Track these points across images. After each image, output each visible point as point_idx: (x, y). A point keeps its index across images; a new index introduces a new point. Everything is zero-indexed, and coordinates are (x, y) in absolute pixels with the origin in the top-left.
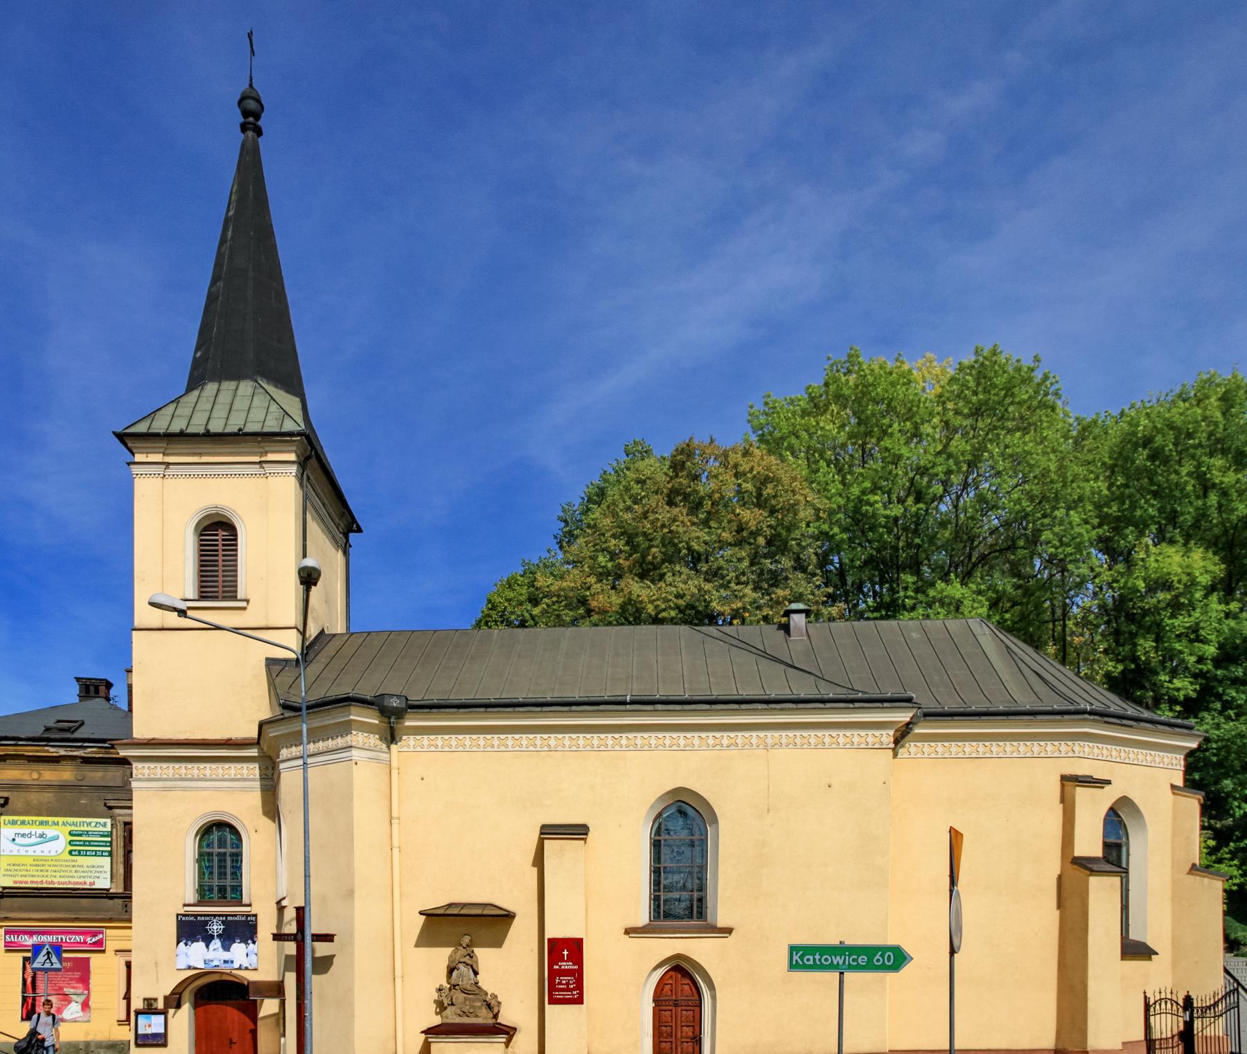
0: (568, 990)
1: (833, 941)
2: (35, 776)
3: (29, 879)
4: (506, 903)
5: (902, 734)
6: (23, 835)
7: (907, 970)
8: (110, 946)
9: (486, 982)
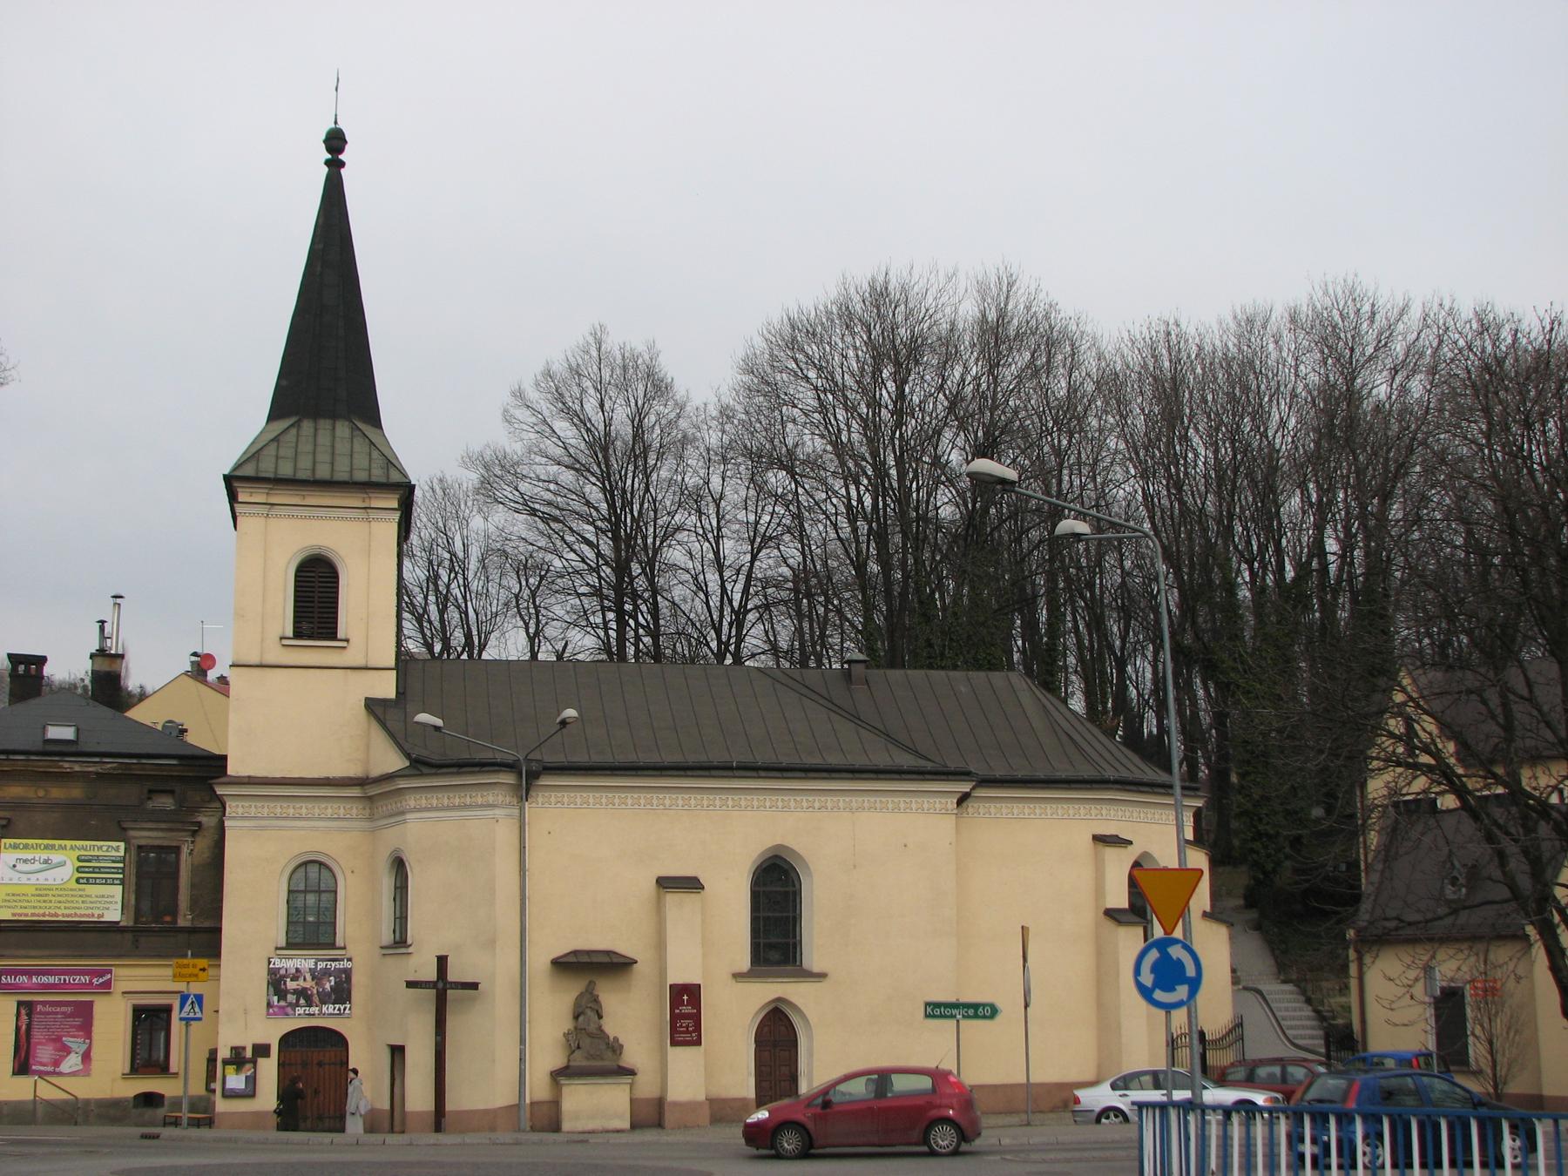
0: (687, 1032)
1: (953, 999)
2: (41, 793)
3: (29, 911)
4: (624, 948)
5: (963, 799)
6: (25, 861)
7: (998, 1018)
8: (119, 986)
9: (611, 1027)
